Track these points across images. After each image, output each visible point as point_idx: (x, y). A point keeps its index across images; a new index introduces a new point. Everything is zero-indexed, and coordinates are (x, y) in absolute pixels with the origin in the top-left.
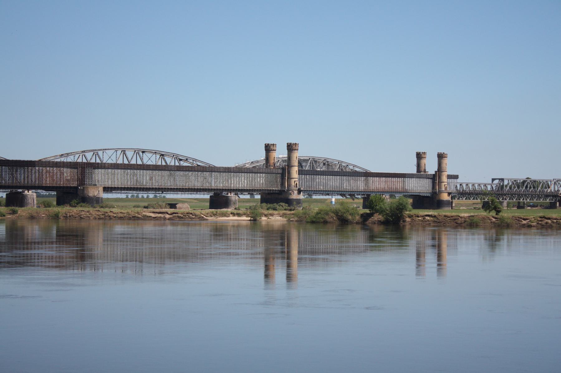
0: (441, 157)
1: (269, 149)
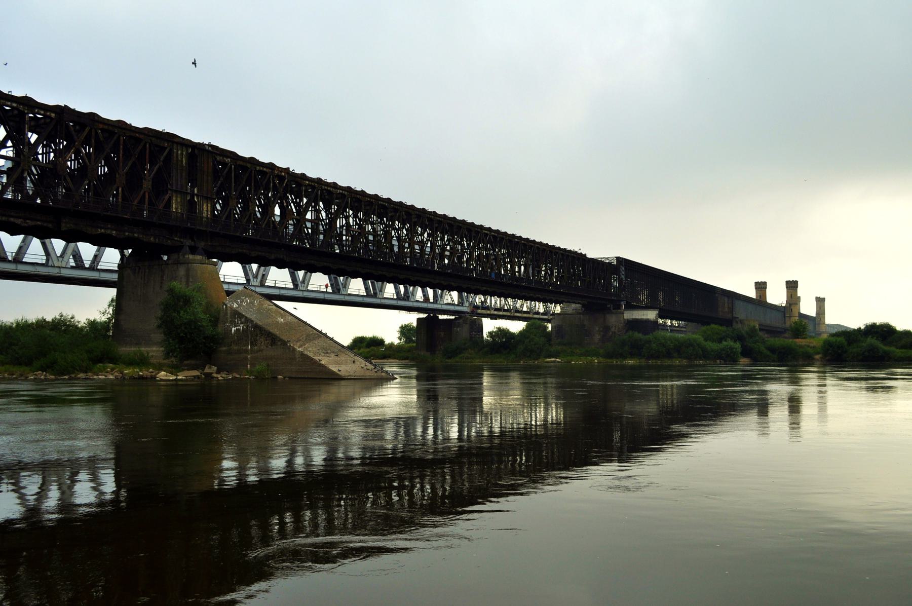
0: (820, 301)
1: (761, 287)
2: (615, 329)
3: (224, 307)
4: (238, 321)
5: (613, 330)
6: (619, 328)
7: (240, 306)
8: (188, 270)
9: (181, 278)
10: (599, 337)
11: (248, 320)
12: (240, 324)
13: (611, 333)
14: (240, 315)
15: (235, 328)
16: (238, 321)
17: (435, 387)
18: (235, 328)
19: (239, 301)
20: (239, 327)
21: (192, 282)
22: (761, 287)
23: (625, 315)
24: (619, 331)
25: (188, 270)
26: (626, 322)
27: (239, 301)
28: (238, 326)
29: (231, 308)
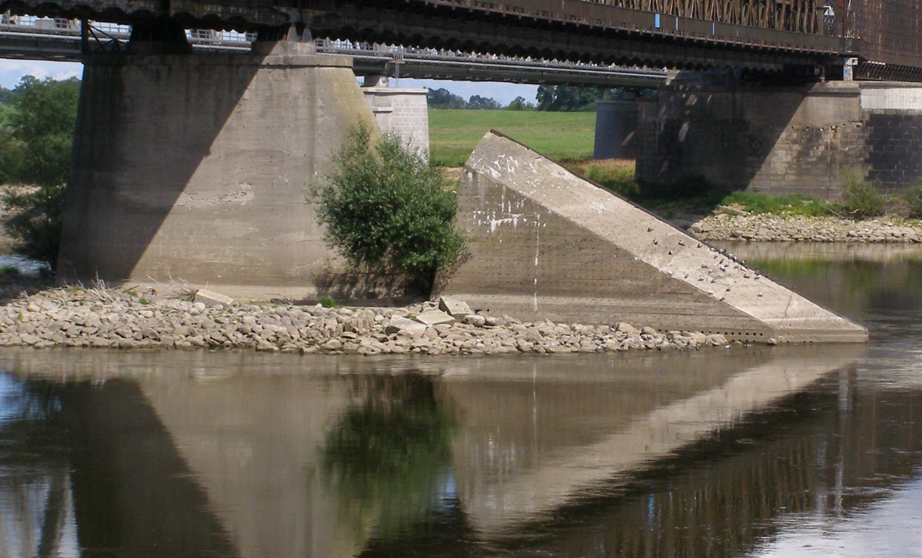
1: (16, 86)
2: (835, 137)
3: (470, 175)
4: (506, 207)
5: (828, 138)
6: (845, 135)
7: (504, 174)
8: (311, 82)
9: (296, 99)
10: (789, 158)
11: (531, 206)
12: (513, 212)
13: (822, 148)
14: (512, 196)
15: (500, 222)
16: (506, 207)
17: (879, 361)
18: (500, 222)
19: (496, 162)
20: (510, 220)
21: (322, 108)
22: (16, 86)
23: (862, 97)
24: (845, 144)
25: (311, 82)
26: (867, 118)
27: (496, 162)
28: (507, 217)
29: (488, 178)
